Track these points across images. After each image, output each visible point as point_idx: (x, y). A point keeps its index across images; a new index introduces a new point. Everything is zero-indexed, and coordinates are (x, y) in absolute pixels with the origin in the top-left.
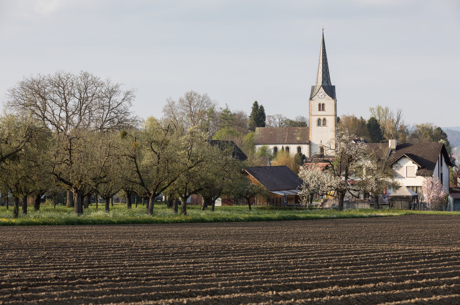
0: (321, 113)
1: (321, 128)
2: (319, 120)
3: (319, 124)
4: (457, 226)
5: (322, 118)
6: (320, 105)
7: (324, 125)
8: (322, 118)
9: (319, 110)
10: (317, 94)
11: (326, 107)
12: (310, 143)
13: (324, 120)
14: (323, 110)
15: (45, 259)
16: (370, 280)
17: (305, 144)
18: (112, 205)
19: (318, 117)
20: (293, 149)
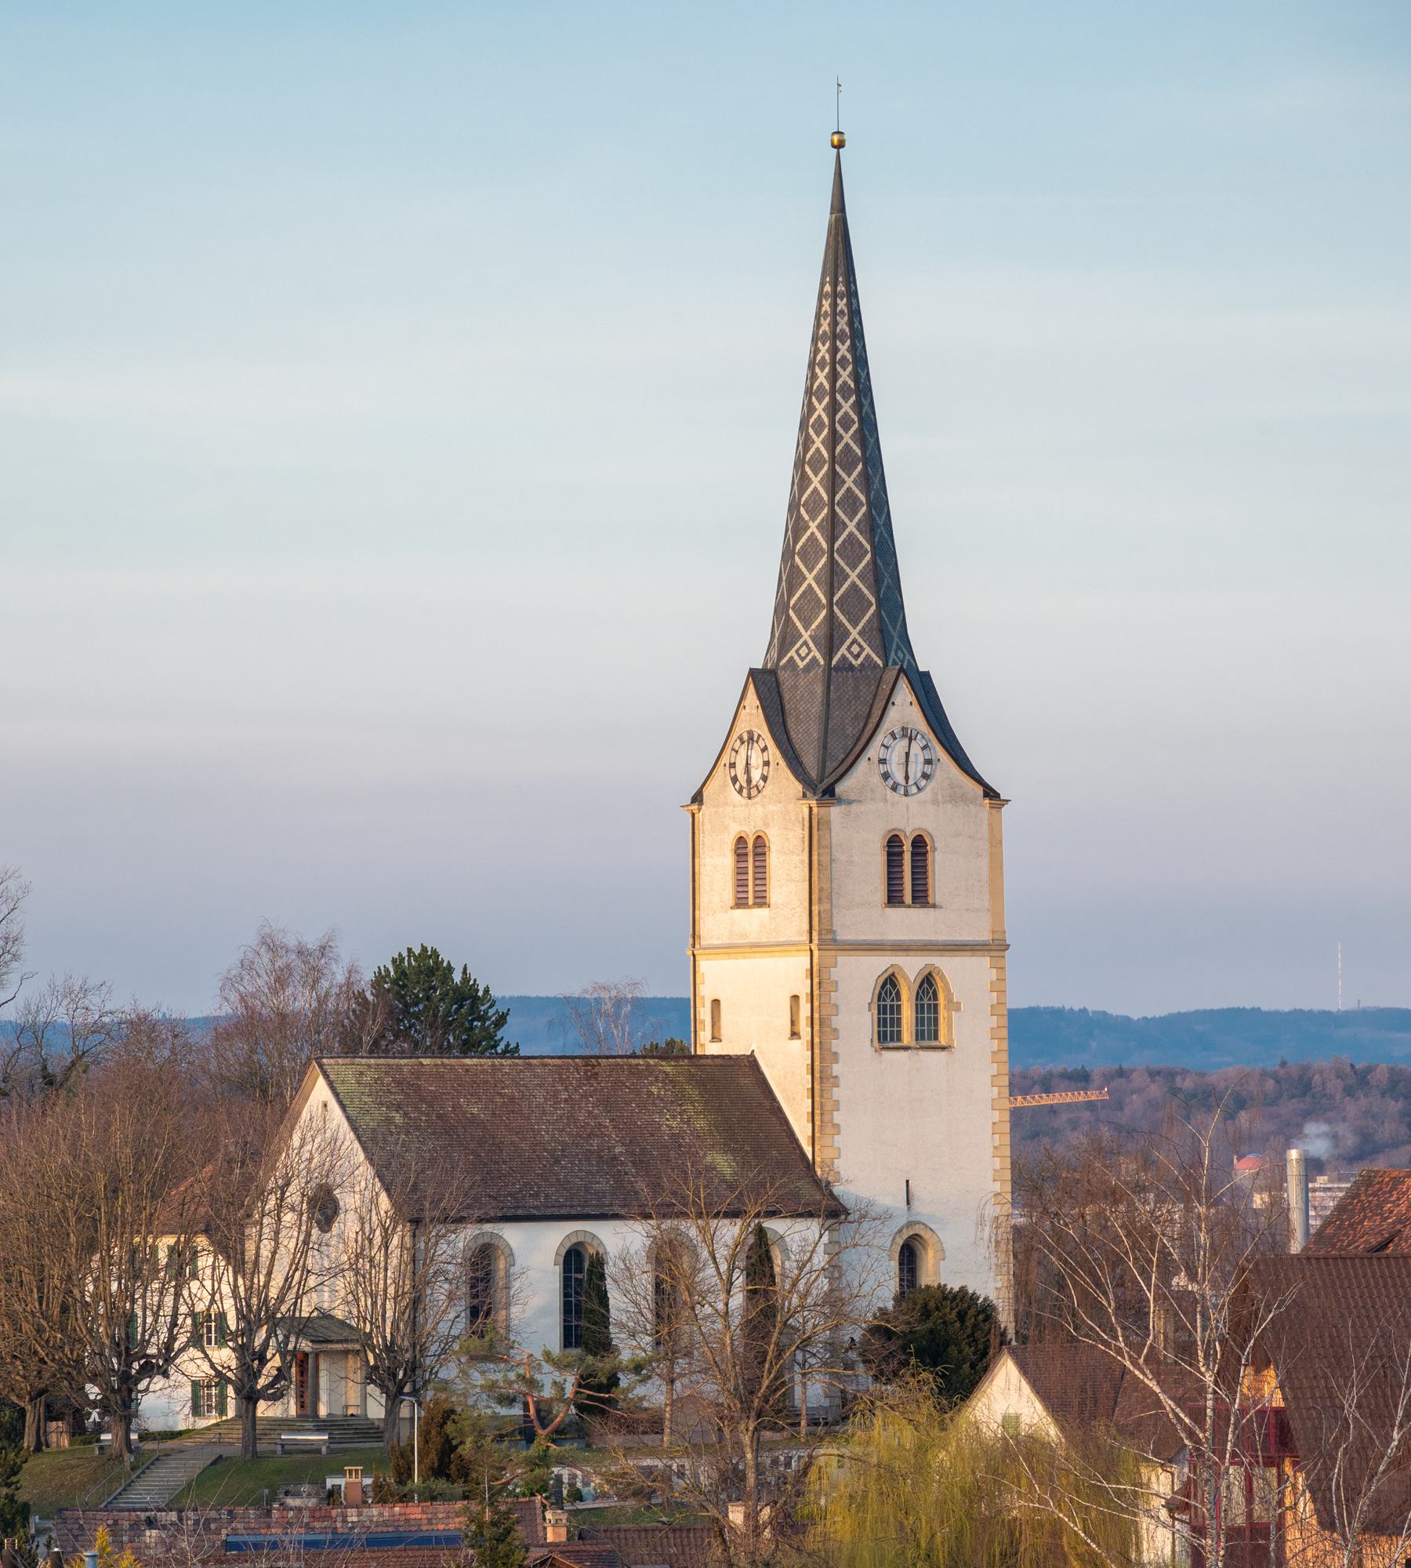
0: (907, 923)
1: (903, 1065)
2: (889, 985)
3: (887, 1034)
6: (893, 844)
7: (928, 1032)
8: (911, 967)
9: (894, 898)
10: (874, 751)
12: (833, 1211)
13: (928, 984)
14: (921, 897)
19: (880, 964)
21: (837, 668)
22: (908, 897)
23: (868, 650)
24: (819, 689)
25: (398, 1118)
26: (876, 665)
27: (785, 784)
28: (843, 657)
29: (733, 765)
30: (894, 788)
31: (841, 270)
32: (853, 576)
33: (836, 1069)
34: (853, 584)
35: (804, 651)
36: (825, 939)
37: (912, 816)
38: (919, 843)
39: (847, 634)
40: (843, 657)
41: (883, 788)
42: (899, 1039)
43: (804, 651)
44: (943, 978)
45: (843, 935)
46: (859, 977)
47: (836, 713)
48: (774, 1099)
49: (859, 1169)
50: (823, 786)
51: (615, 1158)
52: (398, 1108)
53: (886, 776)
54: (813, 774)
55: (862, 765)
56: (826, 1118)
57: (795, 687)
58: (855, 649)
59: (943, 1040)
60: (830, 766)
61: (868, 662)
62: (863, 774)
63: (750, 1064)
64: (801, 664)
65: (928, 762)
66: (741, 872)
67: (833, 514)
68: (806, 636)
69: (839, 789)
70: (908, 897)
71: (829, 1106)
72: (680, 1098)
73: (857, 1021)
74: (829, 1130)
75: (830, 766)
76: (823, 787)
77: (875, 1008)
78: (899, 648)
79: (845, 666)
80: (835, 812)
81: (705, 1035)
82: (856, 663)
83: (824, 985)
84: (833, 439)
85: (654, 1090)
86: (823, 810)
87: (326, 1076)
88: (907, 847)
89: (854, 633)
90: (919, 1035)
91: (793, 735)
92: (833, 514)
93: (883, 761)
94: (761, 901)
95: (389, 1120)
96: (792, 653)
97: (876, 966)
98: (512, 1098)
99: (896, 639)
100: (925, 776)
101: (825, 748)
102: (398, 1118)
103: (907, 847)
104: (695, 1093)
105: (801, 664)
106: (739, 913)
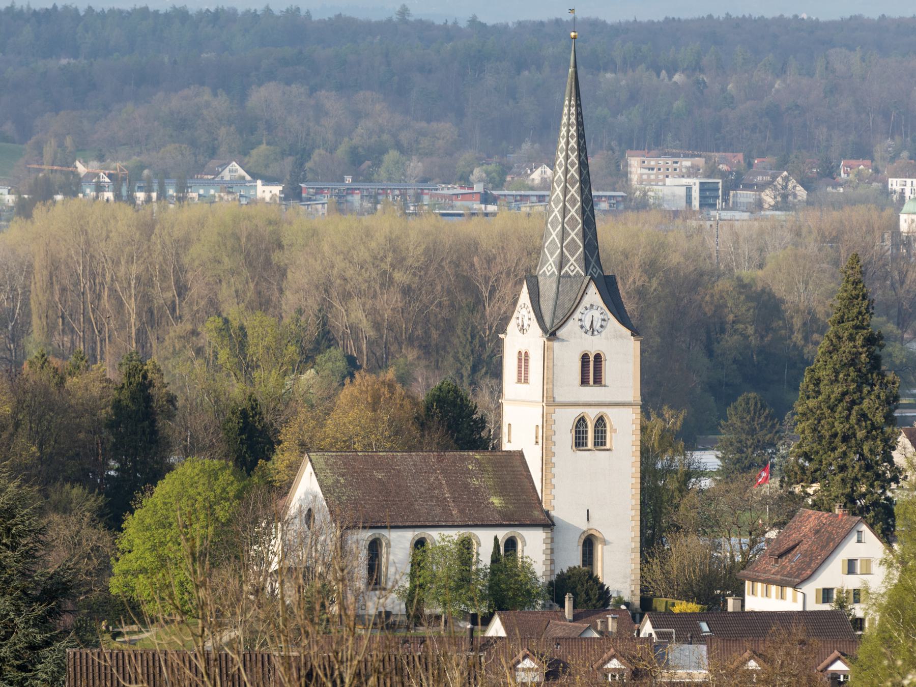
0: (591, 393)
1: (590, 458)
2: (581, 422)
3: (580, 442)
4: (781, 71)
5: (591, 415)
6: (585, 358)
7: (600, 441)
8: (591, 415)
9: (584, 382)
10: (577, 315)
11: (609, 370)
12: (548, 523)
13: (601, 422)
15: (398, 146)
16: (790, 582)
17: (534, 525)
18: (689, 189)
19: (576, 412)
20: (485, 542)
21: (563, 277)
22: (591, 382)
23: (578, 268)
24: (554, 286)
25: (342, 481)
26: (581, 275)
27: (535, 329)
28: (567, 272)
29: (518, 318)
30: (586, 332)
31: (573, 94)
32: (573, 234)
33: (554, 459)
34: (573, 238)
35: (550, 268)
36: (551, 402)
37: (593, 345)
38: (598, 357)
39: (569, 260)
40: (567, 272)
41: (581, 332)
42: (586, 445)
43: (550, 268)
44: (608, 418)
45: (559, 399)
46: (566, 419)
47: (561, 297)
48: (528, 471)
49: (564, 505)
50: (550, 331)
51: (445, 499)
52: (343, 475)
53: (582, 327)
54: (548, 325)
55: (571, 323)
56: (548, 481)
57: (545, 284)
58: (572, 268)
59: (608, 446)
60: (556, 321)
61: (578, 275)
62: (572, 326)
63: (520, 454)
64: (548, 274)
65: (604, 320)
66: (520, 367)
67: (565, 206)
68: (551, 261)
69: (559, 333)
70: (591, 382)
71: (549, 476)
72: (483, 471)
73: (566, 437)
74: (549, 486)
75: (556, 321)
76: (552, 335)
77: (574, 433)
78: (594, 266)
79: (567, 276)
80: (556, 344)
81: (505, 439)
82: (572, 274)
83: (549, 422)
84: (567, 171)
85: (470, 467)
86: (550, 343)
87: (311, 461)
88: (592, 359)
89: (572, 260)
90: (596, 444)
91: (542, 306)
92: (565, 206)
93: (581, 320)
94: (526, 381)
95: (338, 481)
96: (545, 268)
97: (574, 414)
98: (399, 471)
99: (593, 263)
100: (602, 326)
101: (554, 313)
102: (342, 481)
103: (592, 359)
104: (490, 469)
105: (548, 274)
106: (519, 385)
